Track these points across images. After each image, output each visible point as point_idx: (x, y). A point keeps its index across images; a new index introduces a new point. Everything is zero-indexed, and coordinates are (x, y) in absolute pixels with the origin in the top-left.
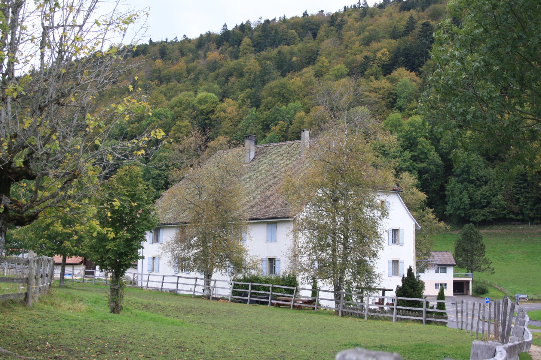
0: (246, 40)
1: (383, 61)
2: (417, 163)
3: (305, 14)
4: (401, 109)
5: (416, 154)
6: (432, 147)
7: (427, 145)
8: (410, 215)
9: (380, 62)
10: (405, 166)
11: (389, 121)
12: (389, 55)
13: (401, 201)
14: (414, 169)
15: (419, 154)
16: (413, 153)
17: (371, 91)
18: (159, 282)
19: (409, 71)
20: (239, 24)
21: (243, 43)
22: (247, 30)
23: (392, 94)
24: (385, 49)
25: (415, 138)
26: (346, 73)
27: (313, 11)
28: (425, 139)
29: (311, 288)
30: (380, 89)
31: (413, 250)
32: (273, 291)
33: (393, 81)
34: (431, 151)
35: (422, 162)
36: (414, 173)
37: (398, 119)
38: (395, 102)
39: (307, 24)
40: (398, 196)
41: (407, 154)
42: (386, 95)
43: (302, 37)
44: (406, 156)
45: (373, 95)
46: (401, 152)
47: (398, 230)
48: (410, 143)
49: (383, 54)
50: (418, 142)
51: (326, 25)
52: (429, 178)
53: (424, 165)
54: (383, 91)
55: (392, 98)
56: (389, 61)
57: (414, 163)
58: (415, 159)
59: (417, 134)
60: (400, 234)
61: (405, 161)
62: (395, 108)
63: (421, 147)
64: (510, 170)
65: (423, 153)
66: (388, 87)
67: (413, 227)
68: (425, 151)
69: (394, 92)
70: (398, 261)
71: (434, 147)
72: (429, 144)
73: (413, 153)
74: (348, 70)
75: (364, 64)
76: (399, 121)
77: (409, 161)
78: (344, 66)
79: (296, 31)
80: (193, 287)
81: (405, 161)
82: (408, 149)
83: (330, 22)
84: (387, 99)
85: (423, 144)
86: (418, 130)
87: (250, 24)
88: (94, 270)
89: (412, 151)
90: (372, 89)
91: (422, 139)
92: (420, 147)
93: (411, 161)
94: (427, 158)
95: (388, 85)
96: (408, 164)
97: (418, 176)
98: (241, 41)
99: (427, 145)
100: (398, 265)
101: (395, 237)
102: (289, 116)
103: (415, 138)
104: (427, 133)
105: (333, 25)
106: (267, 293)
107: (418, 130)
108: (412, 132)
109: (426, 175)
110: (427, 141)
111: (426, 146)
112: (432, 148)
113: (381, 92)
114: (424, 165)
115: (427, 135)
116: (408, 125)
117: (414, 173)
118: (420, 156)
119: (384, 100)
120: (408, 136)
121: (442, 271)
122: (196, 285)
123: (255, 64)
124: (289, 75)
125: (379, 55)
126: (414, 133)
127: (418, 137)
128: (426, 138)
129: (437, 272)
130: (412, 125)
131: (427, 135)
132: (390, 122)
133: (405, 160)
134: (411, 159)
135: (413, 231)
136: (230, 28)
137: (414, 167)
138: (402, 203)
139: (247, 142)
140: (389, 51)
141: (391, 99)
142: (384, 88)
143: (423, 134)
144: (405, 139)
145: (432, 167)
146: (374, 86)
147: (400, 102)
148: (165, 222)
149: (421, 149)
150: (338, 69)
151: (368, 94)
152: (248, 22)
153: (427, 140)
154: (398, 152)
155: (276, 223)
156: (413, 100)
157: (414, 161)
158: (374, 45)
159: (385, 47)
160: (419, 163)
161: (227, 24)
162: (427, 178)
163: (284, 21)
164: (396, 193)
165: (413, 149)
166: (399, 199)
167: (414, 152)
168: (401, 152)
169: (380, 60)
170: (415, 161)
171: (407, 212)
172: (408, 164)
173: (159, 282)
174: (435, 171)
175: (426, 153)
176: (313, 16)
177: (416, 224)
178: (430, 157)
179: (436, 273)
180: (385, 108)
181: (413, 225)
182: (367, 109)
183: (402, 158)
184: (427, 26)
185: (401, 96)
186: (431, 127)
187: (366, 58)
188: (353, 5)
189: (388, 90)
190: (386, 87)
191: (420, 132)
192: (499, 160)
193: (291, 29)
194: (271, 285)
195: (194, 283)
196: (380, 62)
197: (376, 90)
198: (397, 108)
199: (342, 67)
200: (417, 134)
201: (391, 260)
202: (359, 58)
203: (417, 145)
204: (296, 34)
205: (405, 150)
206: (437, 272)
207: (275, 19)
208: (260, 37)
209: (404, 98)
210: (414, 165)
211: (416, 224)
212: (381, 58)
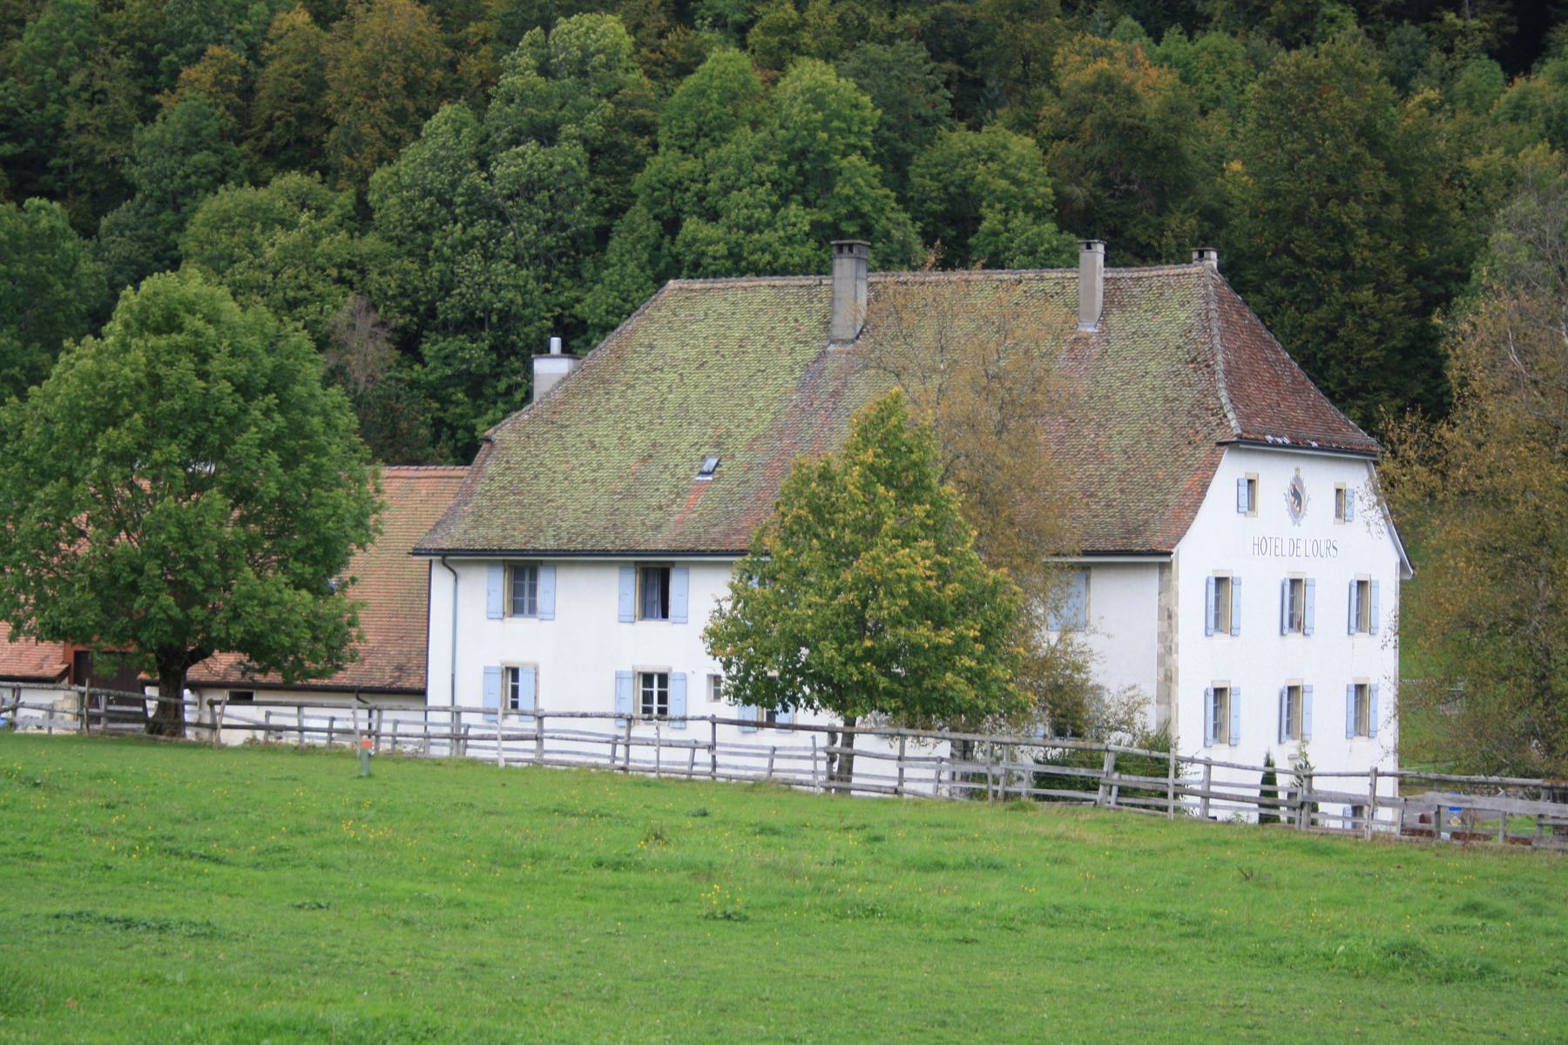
5: (827, 217)
15: (838, 219)
16: (817, 215)
18: (1254, 769)
29: (856, 758)
37: (742, 71)
44: (794, 225)
46: (775, 208)
48: (801, 171)
59: (831, 137)
63: (852, 193)
64: (1341, 332)
73: (817, 215)
80: (908, 773)
85: (859, 180)
86: (836, 124)
88: (164, 699)
102: (247, 26)
103: (824, 156)
106: (984, 787)
107: (836, 124)
108: (815, 129)
111: (867, 190)
122: (900, 759)
127: (836, 151)
139: (844, 266)
143: (852, 140)
144: (785, 157)
148: (609, 547)
149: (848, 199)
154: (763, 208)
155: (1086, 568)
164: (1365, 462)
165: (811, 196)
168: (775, 208)
173: (1254, 769)
179: (486, 668)
191: (840, 130)
192: (1125, 249)
195: (609, 753)
201: (1352, 683)
203: (828, 187)
205: (785, 199)
211: (1402, 563)
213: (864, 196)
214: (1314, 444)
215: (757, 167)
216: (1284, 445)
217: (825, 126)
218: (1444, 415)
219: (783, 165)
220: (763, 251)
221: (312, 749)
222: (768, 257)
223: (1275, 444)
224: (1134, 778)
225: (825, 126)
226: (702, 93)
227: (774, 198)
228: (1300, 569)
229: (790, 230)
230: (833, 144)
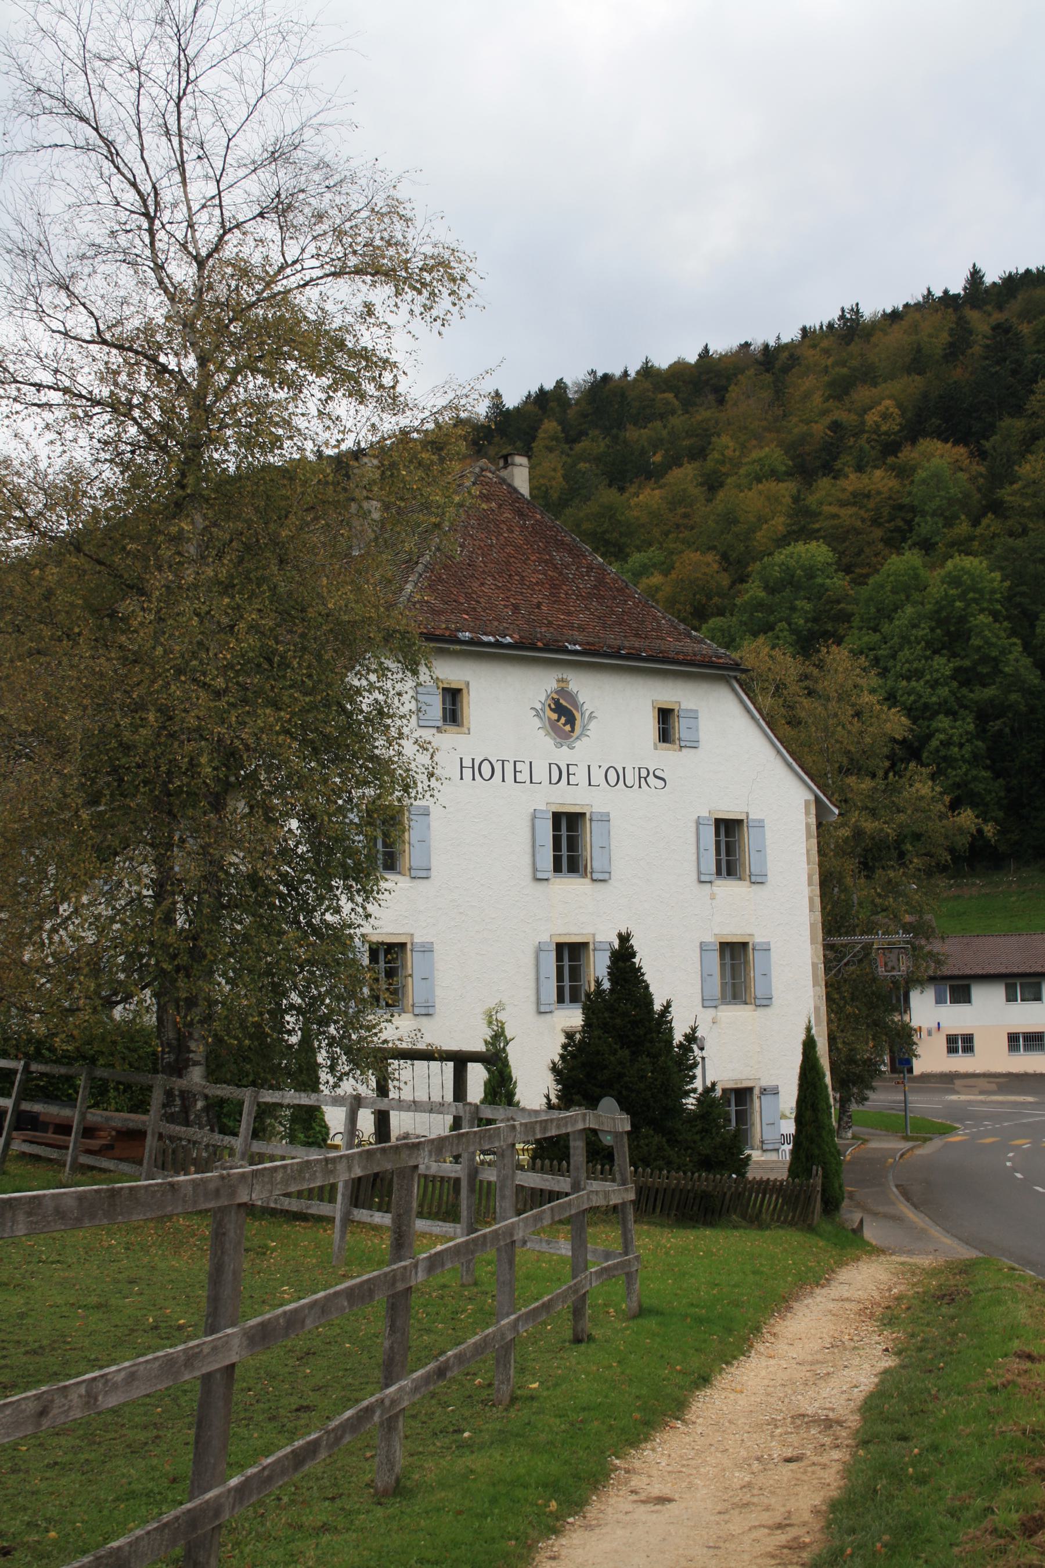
0: (550, 426)
1: (886, 433)
2: (972, 691)
3: (705, 354)
4: (927, 546)
5: (967, 663)
6: (1014, 640)
7: (998, 638)
8: (789, 765)
9: (875, 437)
10: (934, 699)
11: (889, 576)
12: (902, 415)
13: (748, 711)
14: (966, 707)
16: (957, 663)
17: (843, 504)
19: (949, 445)
20: (534, 389)
21: (541, 434)
22: (553, 404)
23: (901, 507)
24: (887, 402)
25: (962, 619)
26: (784, 468)
27: (722, 344)
28: (991, 619)
30: (868, 496)
31: (811, 900)
32: (26, 1094)
33: (903, 472)
34: (1010, 652)
35: (984, 686)
36: (963, 719)
38: (911, 530)
39: (704, 378)
40: (734, 690)
41: (942, 665)
42: (886, 511)
43: (687, 405)
44: (937, 671)
45: (846, 512)
47: (740, 822)
49: (885, 416)
50: (970, 630)
51: (751, 372)
52: (1007, 730)
53: (990, 692)
54: (878, 499)
55: (903, 519)
56: (900, 431)
57: (964, 691)
58: (965, 677)
60: (750, 839)
61: (934, 684)
62: (910, 542)
65: (985, 659)
66: (890, 489)
67: (807, 813)
68: (993, 654)
69: (906, 500)
70: (745, 945)
71: (1018, 642)
72: (1003, 634)
73: (957, 663)
74: (790, 463)
75: (832, 444)
76: (916, 577)
77: (947, 684)
78: (778, 453)
79: (676, 396)
81: (934, 684)
82: (944, 652)
83: (761, 364)
84: (889, 522)
86: (971, 595)
87: (566, 387)
89: (955, 655)
90: (843, 496)
91: (984, 619)
92: (976, 642)
93: (955, 684)
94: (1001, 672)
95: (891, 484)
96: (944, 692)
97: (977, 726)
98: (536, 429)
99: (998, 638)
100: (746, 962)
101: (730, 850)
104: (997, 601)
105: (767, 371)
108: (954, 601)
109: (998, 722)
110: (997, 625)
111: (994, 640)
112: (1015, 644)
113: (871, 505)
114: (990, 692)
115: (999, 607)
116: (943, 583)
117: (963, 719)
118: (979, 669)
119: (880, 525)
120: (944, 614)
121: (1027, 996)
123: (553, 474)
124: (633, 489)
125: (872, 418)
126: (958, 604)
128: (995, 615)
129: (1011, 998)
130: (954, 581)
131: (999, 607)
132: (892, 578)
133: (936, 681)
134: (953, 678)
135: (808, 825)
136: (512, 400)
137: (965, 702)
138: (753, 717)
140: (900, 406)
141: (900, 523)
142: (879, 493)
143: (985, 605)
144: (933, 624)
145: (1014, 697)
146: (850, 489)
147: (925, 527)
150: (760, 459)
151: (833, 509)
152: (560, 385)
153: (996, 621)
156: (959, 518)
157: (962, 684)
158: (862, 394)
159: (889, 397)
160: (977, 688)
161: (501, 392)
162: (1001, 731)
163: (647, 371)
164: (725, 680)
166: (742, 701)
167: (962, 659)
169: (875, 432)
170: (966, 683)
171: (779, 752)
172: (944, 692)
174: (1023, 708)
175: (995, 659)
176: (723, 358)
177: (817, 799)
178: (1007, 669)
179: (1008, 1000)
180: (881, 546)
181: (807, 802)
182: (824, 548)
183: (928, 677)
184: (1007, 331)
185: (927, 508)
186: (1007, 584)
187: (835, 426)
188: (825, 323)
189: (890, 498)
190: (886, 489)
191: (974, 600)
193: (664, 392)
194: (20, 1065)
196: (875, 437)
197: (858, 498)
198: (914, 545)
199: (771, 453)
200: (968, 605)
202: (820, 429)
204: (676, 403)
206: (1011, 998)
207: (626, 374)
208: (586, 416)
209: (934, 514)
210: (964, 696)
211: (817, 800)
212: (878, 426)
213: (991, 645)
214: (540, 644)
215: (914, 632)
216: (509, 646)
217: (962, 597)
218: (839, 645)
219: (932, 630)
220: (909, 695)
221: (198, 1436)
222: (912, 698)
223: (498, 645)
224: (178, 1128)
225: (962, 597)
226: (882, 586)
227: (928, 653)
228: (570, 799)
229: (935, 675)
230: (969, 610)
